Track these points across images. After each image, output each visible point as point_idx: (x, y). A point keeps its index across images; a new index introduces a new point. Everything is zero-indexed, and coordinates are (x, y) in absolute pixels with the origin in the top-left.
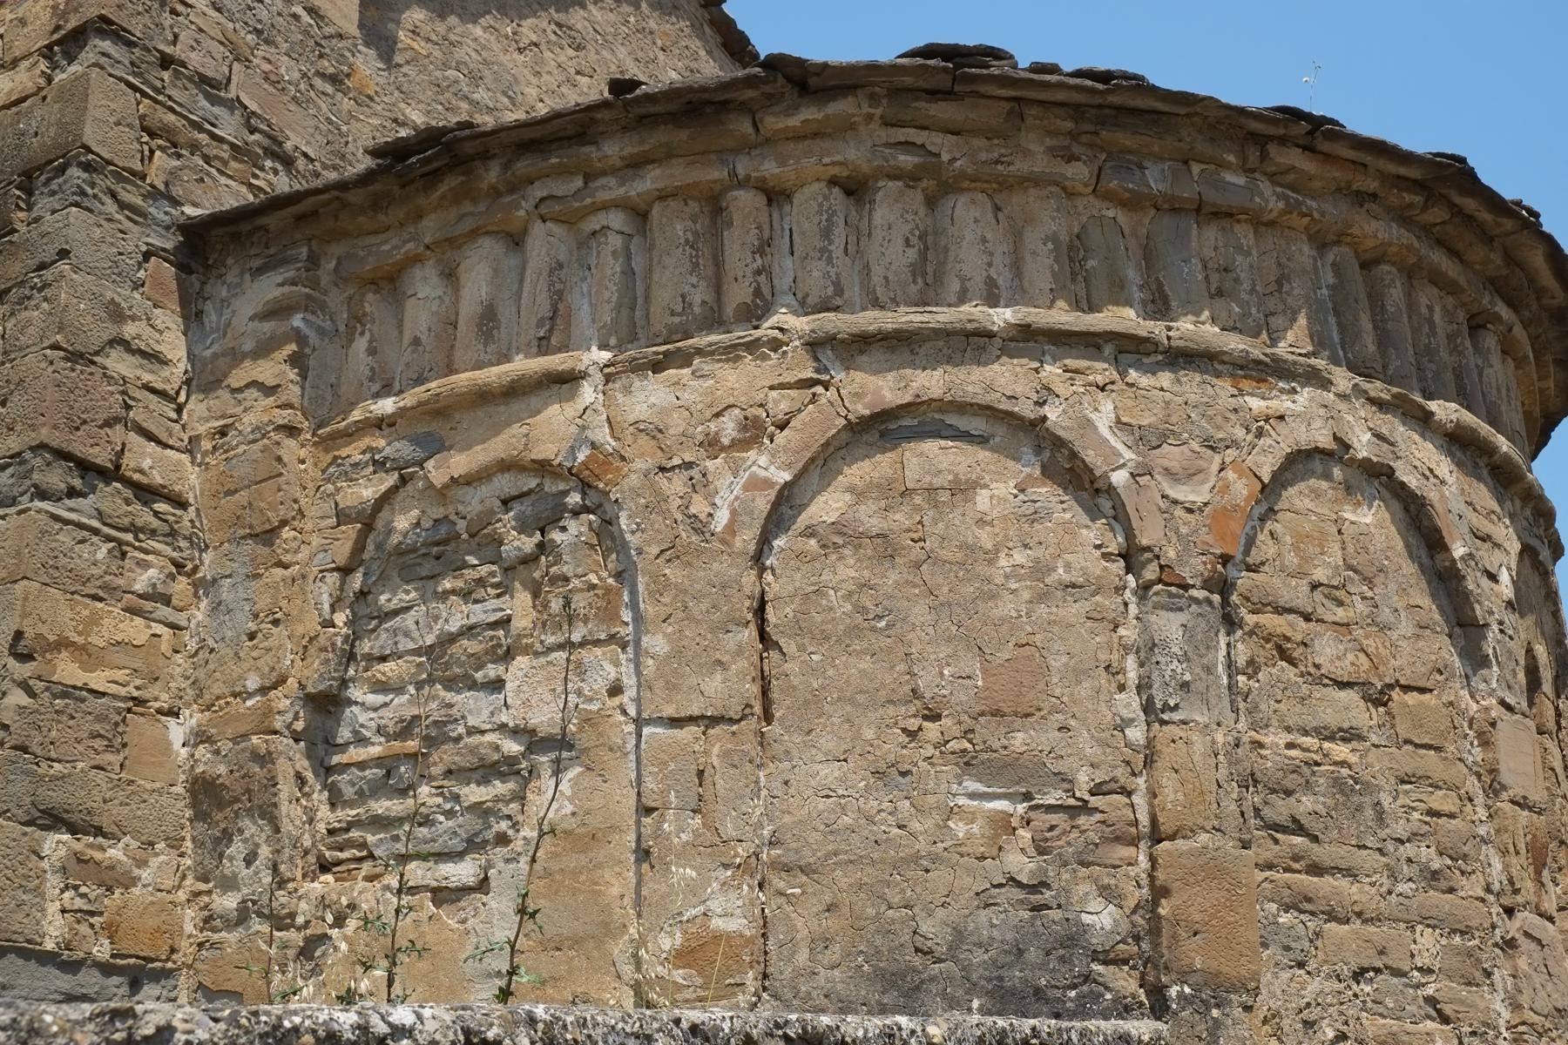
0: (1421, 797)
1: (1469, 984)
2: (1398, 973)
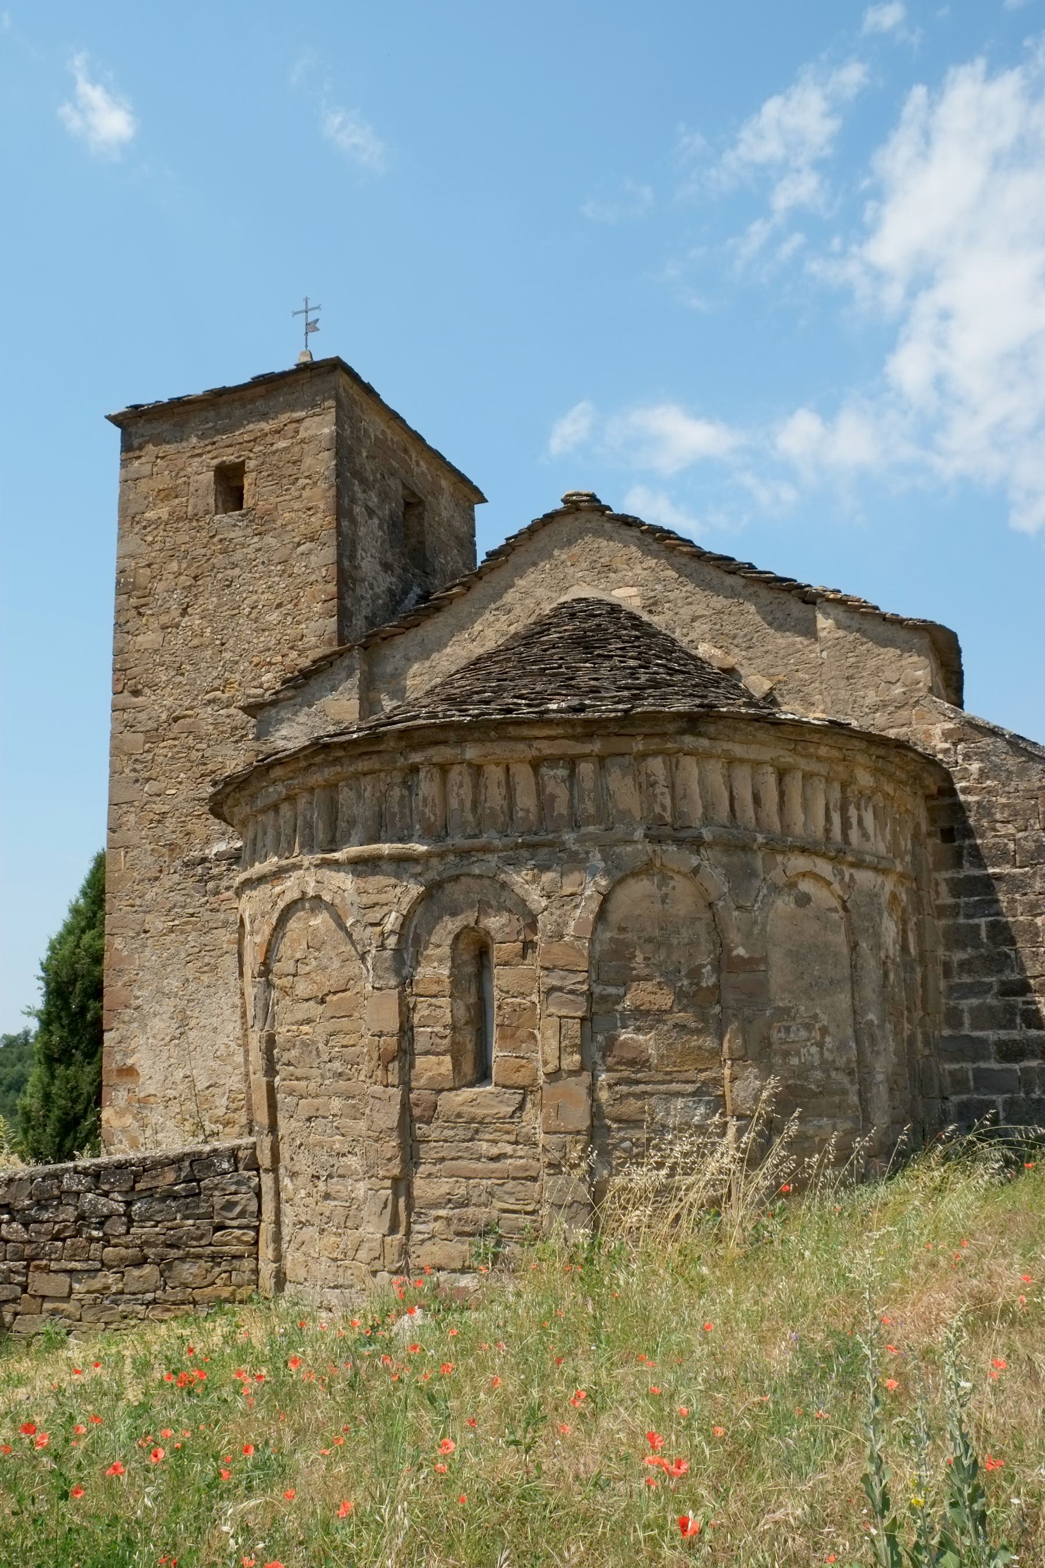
2: (324, 1117)
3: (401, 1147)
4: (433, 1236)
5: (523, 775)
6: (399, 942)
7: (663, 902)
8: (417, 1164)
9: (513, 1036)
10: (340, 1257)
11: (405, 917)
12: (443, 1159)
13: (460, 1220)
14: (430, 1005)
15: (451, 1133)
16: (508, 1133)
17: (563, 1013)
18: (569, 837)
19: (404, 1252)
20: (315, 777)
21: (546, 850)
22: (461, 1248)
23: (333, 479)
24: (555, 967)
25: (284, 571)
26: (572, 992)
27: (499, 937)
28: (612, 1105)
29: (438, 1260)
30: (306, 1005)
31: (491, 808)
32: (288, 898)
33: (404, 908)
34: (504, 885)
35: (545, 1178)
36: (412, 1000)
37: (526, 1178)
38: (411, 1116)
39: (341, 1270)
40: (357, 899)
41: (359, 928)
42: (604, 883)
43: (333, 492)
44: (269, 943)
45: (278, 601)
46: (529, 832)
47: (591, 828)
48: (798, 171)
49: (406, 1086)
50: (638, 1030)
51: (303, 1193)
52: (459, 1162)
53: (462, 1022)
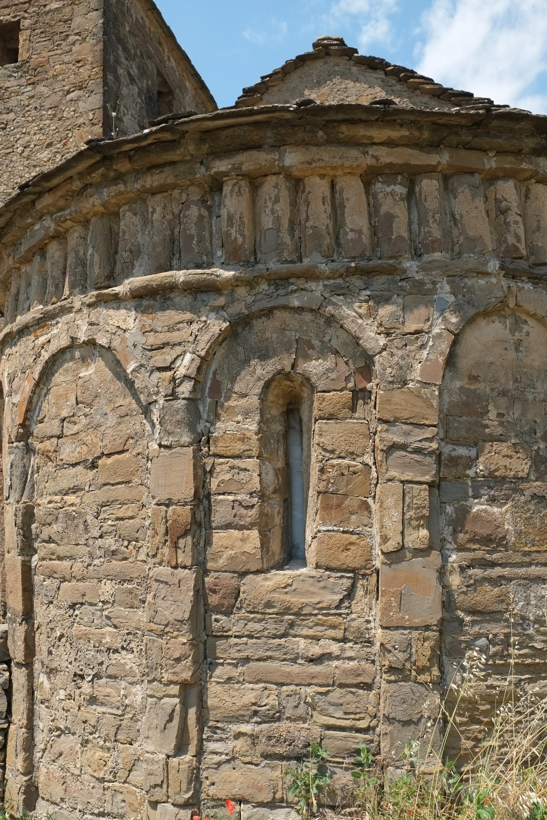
0: (112, 512)
1: (132, 607)
2: (91, 604)
3: (193, 643)
4: (233, 759)
5: (353, 191)
6: (194, 390)
7: (517, 350)
8: (213, 666)
9: (339, 505)
10: (109, 777)
11: (203, 359)
12: (247, 660)
13: (269, 738)
14: (232, 468)
15: (258, 626)
16: (333, 627)
17: (408, 476)
18: (410, 265)
19: (195, 778)
20: (91, 200)
21: (383, 278)
22: (274, 774)
23: (101, 35)
24: (396, 420)
25: (55, 115)
26: (418, 451)
27: (321, 385)
28: (465, 593)
29: (236, 791)
30: (73, 471)
31: (314, 228)
32: (53, 348)
33: (202, 348)
34: (331, 320)
35: (384, 685)
36: (209, 461)
37: (357, 686)
38: (206, 604)
39: (108, 793)
40: (141, 339)
41: (143, 374)
42: (454, 320)
43: (100, 46)
44: (30, 402)
45: (48, 141)
46: (362, 256)
47: (437, 255)
48: (377, 21)
49: (201, 568)
50: (492, 500)
51: (62, 694)
52: (268, 663)
53: (271, 489)
